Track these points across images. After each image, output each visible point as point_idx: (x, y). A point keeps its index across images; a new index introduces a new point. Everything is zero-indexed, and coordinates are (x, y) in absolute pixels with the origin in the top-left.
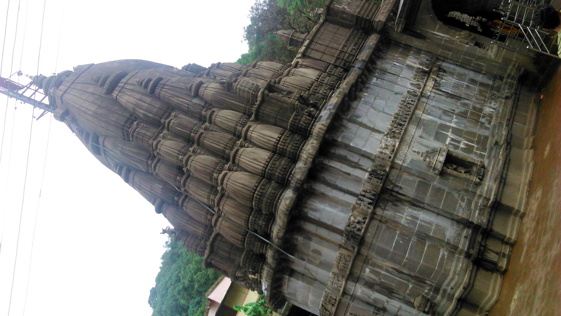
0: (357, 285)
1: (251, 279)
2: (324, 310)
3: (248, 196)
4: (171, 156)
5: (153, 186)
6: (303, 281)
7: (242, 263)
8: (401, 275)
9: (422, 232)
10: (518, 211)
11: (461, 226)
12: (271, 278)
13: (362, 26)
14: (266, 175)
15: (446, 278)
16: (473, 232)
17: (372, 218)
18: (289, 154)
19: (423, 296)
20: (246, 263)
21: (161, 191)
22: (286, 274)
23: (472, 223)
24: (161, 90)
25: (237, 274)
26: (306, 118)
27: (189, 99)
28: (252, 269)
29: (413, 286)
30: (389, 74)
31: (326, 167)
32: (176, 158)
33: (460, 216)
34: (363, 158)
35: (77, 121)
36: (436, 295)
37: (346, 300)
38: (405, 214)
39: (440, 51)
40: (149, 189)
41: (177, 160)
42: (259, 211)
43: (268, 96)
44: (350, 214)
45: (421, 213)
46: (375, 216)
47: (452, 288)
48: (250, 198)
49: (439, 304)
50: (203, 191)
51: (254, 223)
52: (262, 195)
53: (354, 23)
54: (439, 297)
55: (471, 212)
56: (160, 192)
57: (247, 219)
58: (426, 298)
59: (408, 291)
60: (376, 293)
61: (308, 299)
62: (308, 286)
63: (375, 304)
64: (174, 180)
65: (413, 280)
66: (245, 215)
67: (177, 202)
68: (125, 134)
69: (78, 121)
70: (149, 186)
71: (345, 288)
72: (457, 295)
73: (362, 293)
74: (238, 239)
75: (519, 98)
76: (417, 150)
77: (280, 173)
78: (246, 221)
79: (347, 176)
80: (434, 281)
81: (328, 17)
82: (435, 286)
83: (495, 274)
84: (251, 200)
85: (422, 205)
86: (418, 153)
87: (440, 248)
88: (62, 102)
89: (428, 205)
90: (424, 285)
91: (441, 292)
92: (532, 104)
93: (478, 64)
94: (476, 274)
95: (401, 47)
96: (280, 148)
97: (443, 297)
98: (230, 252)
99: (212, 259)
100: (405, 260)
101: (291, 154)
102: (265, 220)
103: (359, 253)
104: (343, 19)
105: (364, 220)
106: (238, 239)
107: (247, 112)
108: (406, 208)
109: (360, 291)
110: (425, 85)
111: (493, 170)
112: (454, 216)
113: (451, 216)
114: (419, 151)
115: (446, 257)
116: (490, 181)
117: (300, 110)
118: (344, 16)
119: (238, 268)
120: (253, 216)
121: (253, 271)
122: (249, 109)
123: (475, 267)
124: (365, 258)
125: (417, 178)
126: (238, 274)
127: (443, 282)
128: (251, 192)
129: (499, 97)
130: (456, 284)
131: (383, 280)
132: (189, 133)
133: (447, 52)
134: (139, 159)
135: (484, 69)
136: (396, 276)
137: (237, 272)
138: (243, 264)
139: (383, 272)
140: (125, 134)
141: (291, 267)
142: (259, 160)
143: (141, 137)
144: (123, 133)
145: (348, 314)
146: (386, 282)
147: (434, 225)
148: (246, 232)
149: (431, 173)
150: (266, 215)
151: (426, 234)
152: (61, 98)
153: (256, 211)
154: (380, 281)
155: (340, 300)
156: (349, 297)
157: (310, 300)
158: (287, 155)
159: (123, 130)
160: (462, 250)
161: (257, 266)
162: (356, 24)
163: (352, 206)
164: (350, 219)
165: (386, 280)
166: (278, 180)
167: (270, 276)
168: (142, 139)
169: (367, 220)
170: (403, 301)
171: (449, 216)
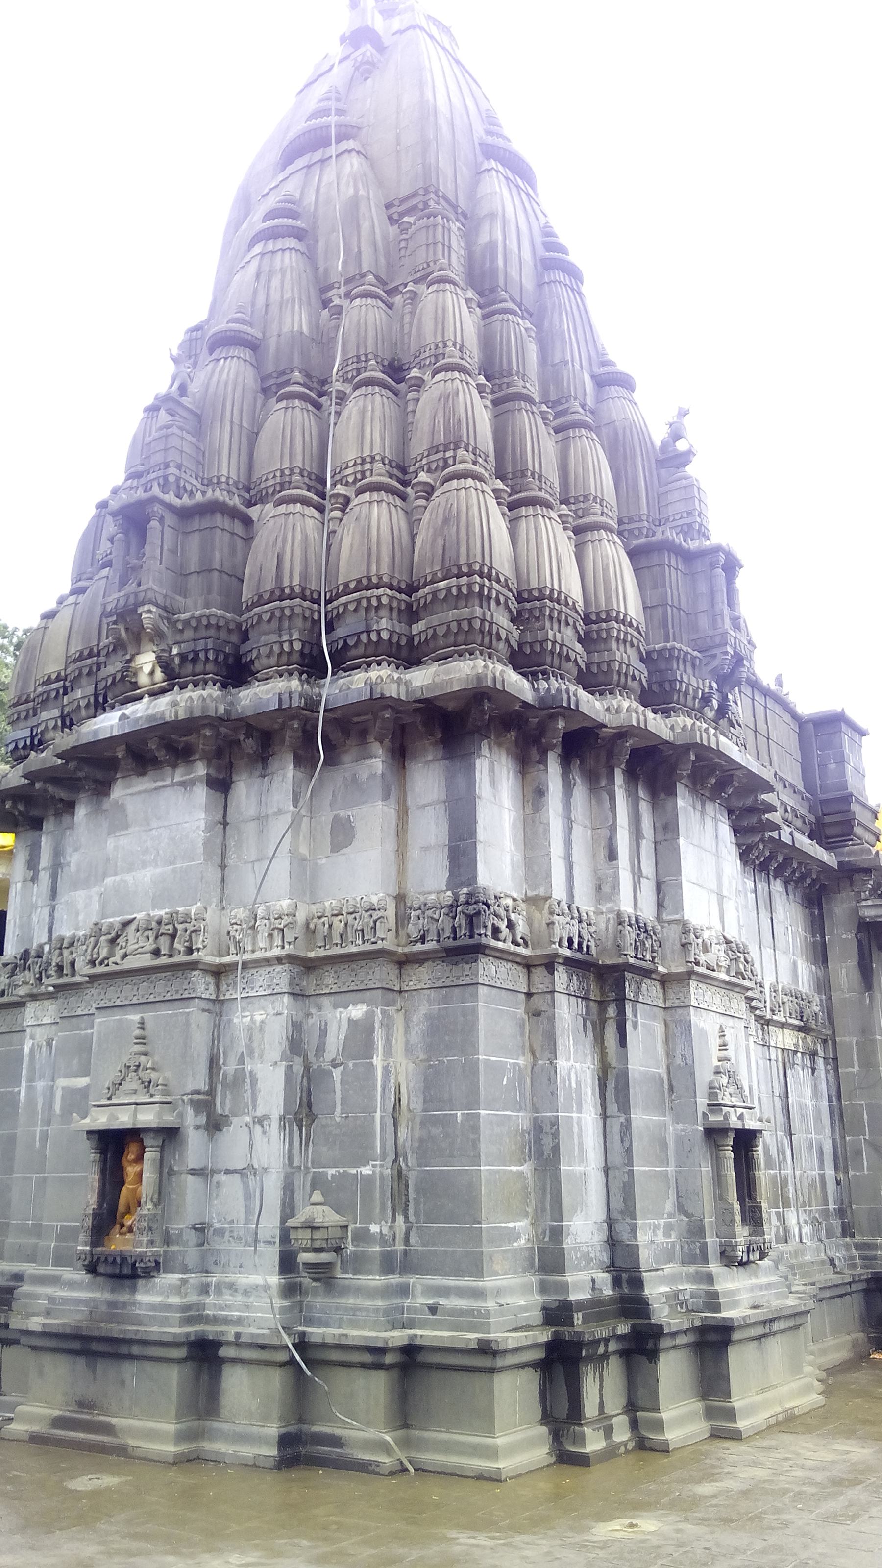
0: (286, 998)
1: (133, 665)
2: (110, 937)
3: (463, 560)
4: (440, 327)
5: (297, 307)
6: (209, 828)
7: (192, 617)
8: (390, 1121)
9: (556, 1135)
10: (731, 1414)
11: (605, 1258)
12: (197, 713)
13: (827, 819)
14: (528, 605)
15: (458, 1272)
16: (612, 1300)
17: (528, 965)
18: (599, 664)
19: (347, 1227)
20: (196, 629)
21: (292, 332)
22: (209, 766)
23: (637, 1283)
24: (565, 285)
25: (146, 607)
26: (698, 688)
27: (584, 363)
28: (183, 657)
29: (368, 1180)
30: (770, 921)
31: (603, 783)
32: (439, 339)
33: (636, 1238)
34: (655, 888)
35: (366, 79)
36: (376, 1266)
37: (202, 985)
38: (578, 1065)
39: (848, 1039)
40: (275, 296)
41: (433, 347)
42: (411, 614)
43: (713, 566)
44: (515, 895)
45: (593, 1115)
46: (539, 974)
47: (433, 1309)
48: (459, 567)
49: (345, 1291)
50: (383, 439)
51: (367, 609)
52: (483, 598)
53: (823, 797)
54: (376, 1280)
55: (657, 1270)
56: (286, 329)
57: (375, 580)
58: (343, 1238)
59: (331, 1171)
60: (281, 1071)
61: (130, 868)
62: (201, 850)
63: (219, 1087)
64: (358, 357)
65: (389, 1171)
66: (385, 569)
67: (287, 383)
68: (414, 201)
69: (369, 81)
70: (288, 295)
71: (233, 967)
72: (427, 1335)
73: (250, 1029)
74: (279, 576)
75: (845, 1294)
76: (727, 1038)
77: (554, 643)
78: (365, 582)
79: (602, 853)
80: (412, 1240)
81: (811, 725)
82: (395, 1251)
83: (544, 1429)
84: (455, 571)
85: (612, 1108)
86: (723, 1046)
87: (526, 1214)
88: (401, 32)
89: (627, 1127)
90: (390, 1213)
91: (394, 1279)
92: (848, 1338)
93: (859, 1153)
94: (522, 1366)
95: (814, 936)
96: (608, 630)
97: (386, 1292)
98: (210, 571)
99: (161, 520)
100: (459, 1113)
101: (605, 668)
102: (395, 639)
103: (404, 962)
104: (823, 766)
105: (521, 941)
106: (279, 576)
107: (627, 527)
108: (589, 1063)
109: (258, 1018)
110: (782, 1025)
111: (761, 1288)
112: (628, 1220)
113: (622, 1212)
114: (731, 1047)
115: (515, 1244)
116: (752, 1289)
117: (710, 668)
118: (832, 766)
119: (165, 609)
120: (391, 598)
121: (177, 660)
122: (640, 529)
123: (540, 1354)
124: (397, 988)
125: (665, 1067)
126: (150, 611)
127: (435, 1272)
128: (483, 565)
129: (820, 1240)
130: (461, 1312)
131: (337, 1073)
132: (514, 372)
133: (855, 1059)
134: (360, 252)
135: (851, 1173)
136: (383, 1110)
137: (154, 609)
138: (187, 623)
139: (378, 1061)
140: (414, 201)
141: (235, 778)
142: (562, 572)
143: (440, 238)
144: (414, 195)
145: (135, 1017)
146: (338, 1087)
147: (582, 1168)
148: (315, 596)
149: (702, 1102)
150: (411, 639)
151: (556, 1149)
152: (414, 27)
153: (409, 606)
154: (326, 1066)
155: (193, 965)
156: (211, 993)
157: (129, 877)
158: (596, 657)
159: (421, 192)
160: (564, 1288)
161: (199, 667)
162: (823, 802)
163: (542, 891)
164: (507, 896)
165: (342, 1083)
166: (531, 644)
167: (204, 708)
168: (435, 244)
169: (521, 950)
170: (289, 1170)
171: (617, 1203)
